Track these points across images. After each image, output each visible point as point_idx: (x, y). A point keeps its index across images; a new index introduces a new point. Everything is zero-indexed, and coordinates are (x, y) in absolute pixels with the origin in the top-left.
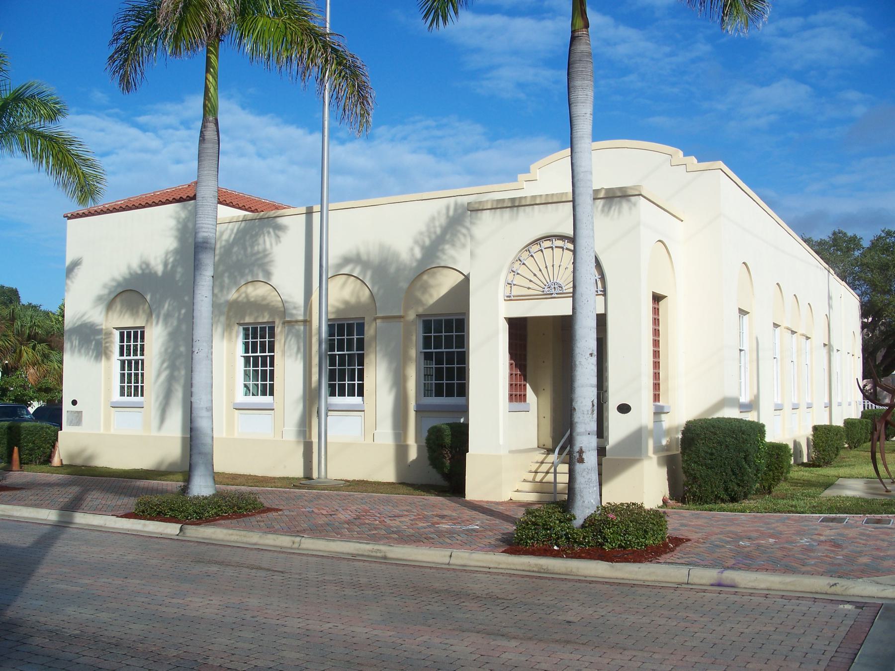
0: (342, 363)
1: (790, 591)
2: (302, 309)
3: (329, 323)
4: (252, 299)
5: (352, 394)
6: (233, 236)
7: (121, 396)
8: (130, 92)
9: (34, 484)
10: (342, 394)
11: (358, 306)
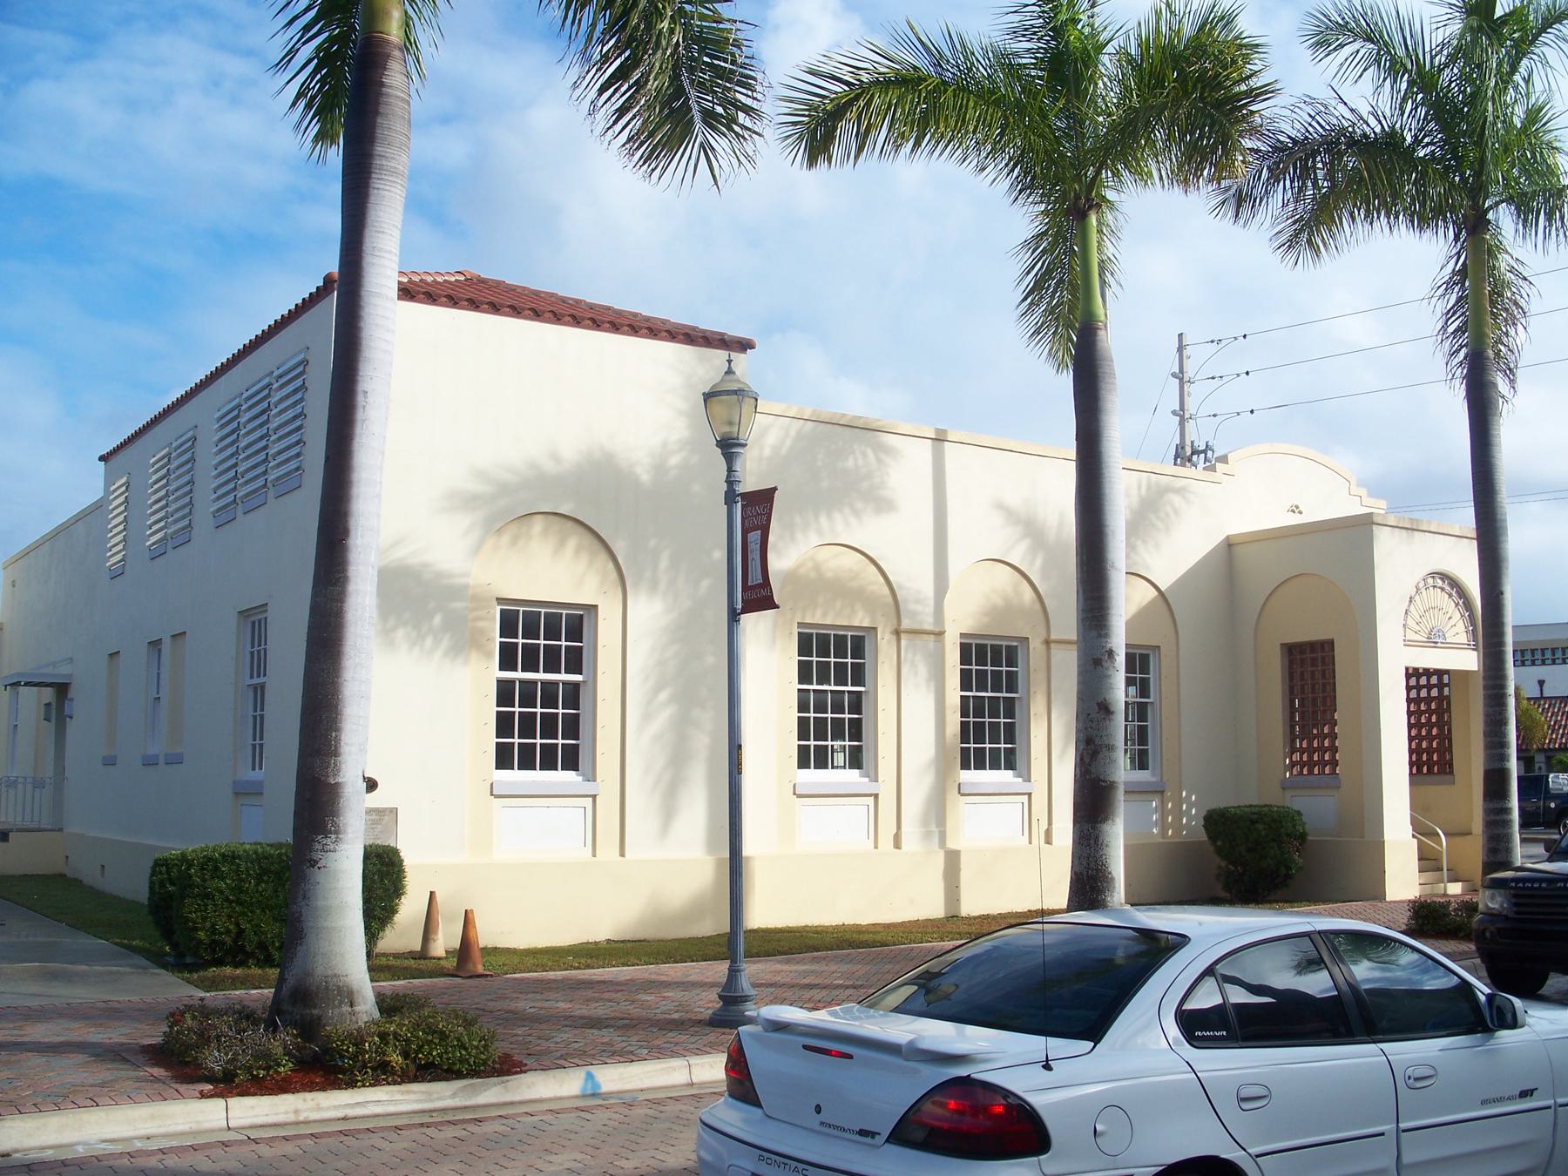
0: (820, 707)
1: (261, 1126)
2: (932, 602)
3: (964, 641)
4: (829, 575)
5: (995, 766)
6: (788, 443)
7: (498, 767)
8: (1395, 231)
9: (97, 1055)
10: (980, 765)
11: (1006, 610)
